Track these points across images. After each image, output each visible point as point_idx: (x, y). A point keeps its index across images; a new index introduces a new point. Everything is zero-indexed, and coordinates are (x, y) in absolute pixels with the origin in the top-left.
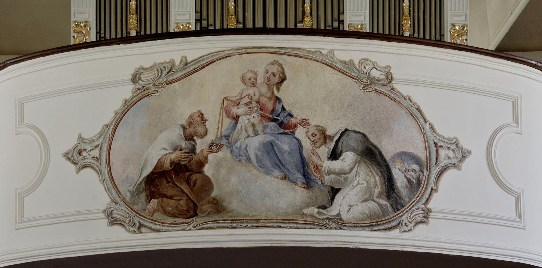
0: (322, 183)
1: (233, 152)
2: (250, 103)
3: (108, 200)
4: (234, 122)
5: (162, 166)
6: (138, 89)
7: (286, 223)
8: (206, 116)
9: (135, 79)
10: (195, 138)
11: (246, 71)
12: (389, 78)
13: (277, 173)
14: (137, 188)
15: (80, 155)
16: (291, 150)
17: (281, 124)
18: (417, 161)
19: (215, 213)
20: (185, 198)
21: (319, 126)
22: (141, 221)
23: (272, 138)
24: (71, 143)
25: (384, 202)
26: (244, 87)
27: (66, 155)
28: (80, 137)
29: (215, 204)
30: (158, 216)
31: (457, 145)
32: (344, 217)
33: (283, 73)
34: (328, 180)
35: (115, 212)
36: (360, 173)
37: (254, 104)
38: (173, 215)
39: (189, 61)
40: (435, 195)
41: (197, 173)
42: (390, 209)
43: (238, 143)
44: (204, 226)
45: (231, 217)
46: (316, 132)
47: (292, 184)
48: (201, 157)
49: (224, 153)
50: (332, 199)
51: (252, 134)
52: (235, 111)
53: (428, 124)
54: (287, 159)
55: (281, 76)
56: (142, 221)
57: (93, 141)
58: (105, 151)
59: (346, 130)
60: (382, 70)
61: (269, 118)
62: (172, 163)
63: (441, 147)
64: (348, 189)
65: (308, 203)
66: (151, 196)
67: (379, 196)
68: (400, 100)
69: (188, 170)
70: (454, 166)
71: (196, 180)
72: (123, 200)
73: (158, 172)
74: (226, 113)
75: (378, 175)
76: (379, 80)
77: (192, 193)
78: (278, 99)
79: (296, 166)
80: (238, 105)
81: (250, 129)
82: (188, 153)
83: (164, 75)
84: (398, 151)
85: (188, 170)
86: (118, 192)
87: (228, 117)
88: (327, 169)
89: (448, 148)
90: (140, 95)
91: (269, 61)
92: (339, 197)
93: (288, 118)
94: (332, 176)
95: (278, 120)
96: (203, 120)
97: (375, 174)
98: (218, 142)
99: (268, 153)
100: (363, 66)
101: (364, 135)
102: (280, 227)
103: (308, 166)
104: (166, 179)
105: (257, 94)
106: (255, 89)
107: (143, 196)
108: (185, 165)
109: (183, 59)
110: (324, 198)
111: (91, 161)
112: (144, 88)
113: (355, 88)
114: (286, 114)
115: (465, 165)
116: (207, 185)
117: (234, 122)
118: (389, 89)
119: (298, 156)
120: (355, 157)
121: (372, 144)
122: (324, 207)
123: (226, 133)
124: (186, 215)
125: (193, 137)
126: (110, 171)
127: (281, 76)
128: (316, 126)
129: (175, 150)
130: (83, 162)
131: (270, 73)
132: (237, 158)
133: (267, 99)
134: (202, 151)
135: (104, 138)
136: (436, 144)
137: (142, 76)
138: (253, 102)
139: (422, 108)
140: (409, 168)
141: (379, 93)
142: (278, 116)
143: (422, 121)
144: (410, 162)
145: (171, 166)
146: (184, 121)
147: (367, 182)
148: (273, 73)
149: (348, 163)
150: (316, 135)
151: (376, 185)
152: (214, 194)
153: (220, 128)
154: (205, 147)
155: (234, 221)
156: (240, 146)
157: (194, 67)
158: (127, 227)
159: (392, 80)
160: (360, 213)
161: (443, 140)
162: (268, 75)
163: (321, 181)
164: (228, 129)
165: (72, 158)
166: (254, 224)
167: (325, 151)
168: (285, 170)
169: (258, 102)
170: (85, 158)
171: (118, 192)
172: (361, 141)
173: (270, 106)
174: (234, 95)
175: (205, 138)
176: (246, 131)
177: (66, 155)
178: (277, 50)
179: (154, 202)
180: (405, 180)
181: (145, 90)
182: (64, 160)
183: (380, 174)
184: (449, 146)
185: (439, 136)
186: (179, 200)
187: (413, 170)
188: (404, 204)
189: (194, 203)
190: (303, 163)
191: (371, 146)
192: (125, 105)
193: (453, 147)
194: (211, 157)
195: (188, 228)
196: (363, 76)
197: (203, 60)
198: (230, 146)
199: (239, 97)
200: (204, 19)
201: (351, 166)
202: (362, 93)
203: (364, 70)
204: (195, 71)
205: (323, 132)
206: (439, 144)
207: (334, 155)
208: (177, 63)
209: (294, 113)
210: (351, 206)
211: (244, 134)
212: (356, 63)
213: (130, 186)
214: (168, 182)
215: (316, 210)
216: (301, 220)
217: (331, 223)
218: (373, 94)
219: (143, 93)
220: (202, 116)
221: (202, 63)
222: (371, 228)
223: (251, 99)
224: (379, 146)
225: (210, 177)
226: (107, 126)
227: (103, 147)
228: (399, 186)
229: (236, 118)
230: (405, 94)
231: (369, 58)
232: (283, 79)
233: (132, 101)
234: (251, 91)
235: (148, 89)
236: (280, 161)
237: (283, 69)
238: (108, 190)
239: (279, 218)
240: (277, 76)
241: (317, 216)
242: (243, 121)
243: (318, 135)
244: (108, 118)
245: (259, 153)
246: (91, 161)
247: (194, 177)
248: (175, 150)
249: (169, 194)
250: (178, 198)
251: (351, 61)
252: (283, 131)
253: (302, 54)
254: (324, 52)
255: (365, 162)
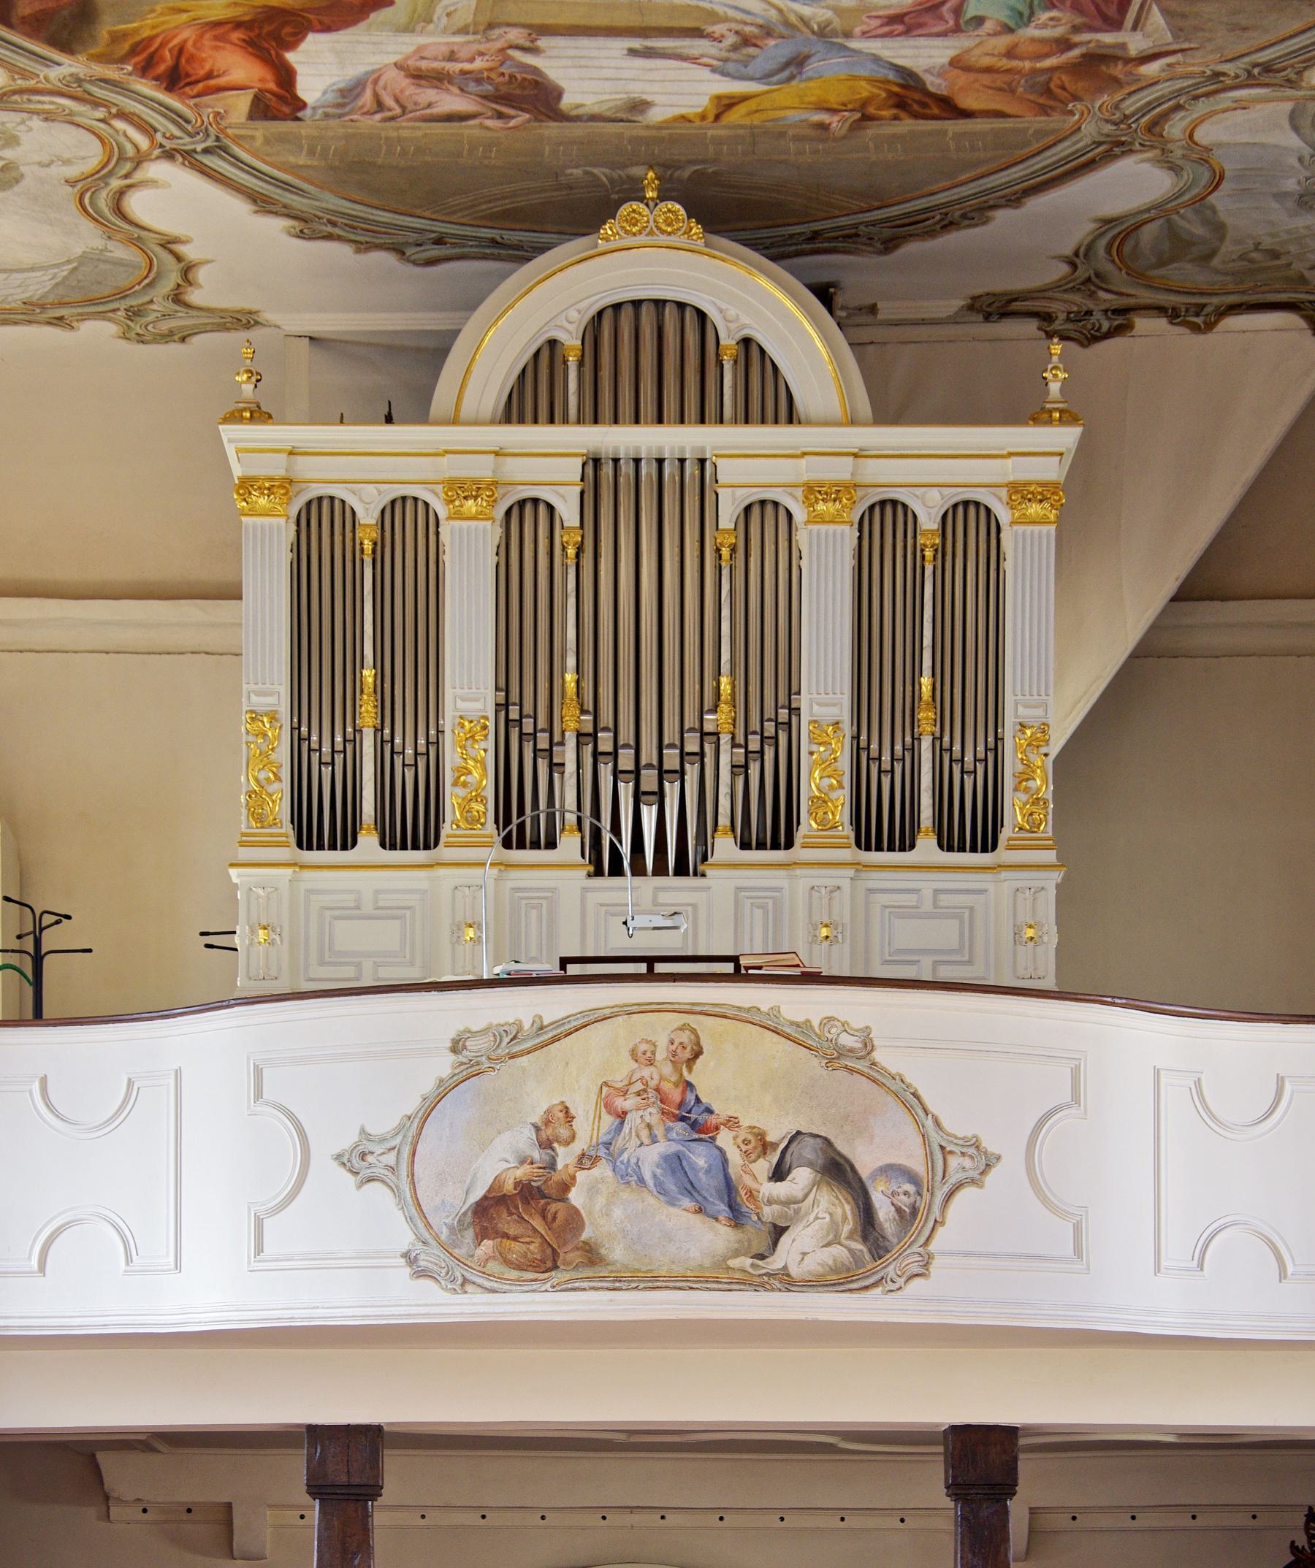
0: (759, 1219)
1: (617, 1170)
2: (645, 1091)
3: (410, 1237)
4: (618, 1121)
5: (501, 1187)
6: (462, 1064)
7: (700, 1282)
8: (572, 1111)
9: (457, 1047)
10: (555, 1145)
11: (638, 1040)
12: (868, 1046)
13: (687, 1203)
14: (459, 1221)
15: (363, 1160)
16: (710, 1166)
17: (694, 1126)
18: (913, 1178)
19: (587, 1266)
20: (538, 1240)
21: (754, 1127)
22: (465, 1273)
23: (680, 1147)
24: (347, 1140)
25: (858, 1246)
26: (636, 1065)
27: (338, 1157)
28: (363, 1131)
29: (587, 1251)
30: (494, 1267)
31: (977, 1147)
32: (795, 1271)
33: (698, 1044)
34: (769, 1212)
35: (422, 1257)
36: (819, 1202)
37: (651, 1093)
38: (519, 1268)
39: (545, 1023)
40: (940, 1231)
41: (559, 1200)
42: (867, 1257)
43: (625, 1155)
44: (569, 1286)
45: (612, 1271)
46: (750, 1137)
47: (711, 1220)
48: (565, 1177)
49: (602, 1171)
50: (775, 1243)
51: (646, 1141)
52: (620, 1103)
53: (930, 1116)
54: (702, 1179)
55: (695, 1048)
56: (468, 1275)
57: (383, 1140)
58: (406, 1156)
59: (799, 1133)
60: (856, 1033)
61: (674, 1115)
62: (517, 1183)
63: (951, 1152)
64: (800, 1227)
65: (737, 1250)
66: (482, 1235)
67: (849, 1237)
68: (885, 1081)
69: (544, 1197)
70: (973, 1182)
71: (556, 1213)
72: (436, 1237)
73: (494, 1197)
74: (606, 1106)
75: (848, 1203)
76: (851, 1050)
77: (549, 1232)
78: (689, 1085)
79: (718, 1191)
80: (625, 1093)
81: (644, 1134)
82: (544, 1168)
83: (504, 1043)
84: (880, 1164)
85: (544, 1197)
86: (428, 1225)
87: (609, 1113)
88: (767, 1195)
89: (963, 1154)
90: (465, 1073)
91: (676, 1025)
92: (785, 1240)
93: (705, 1116)
94: (776, 1207)
95: (689, 1118)
96: (569, 1117)
97: (843, 1201)
98: (592, 1153)
99: (673, 1172)
100: (826, 1029)
101: (827, 1140)
102: (691, 1288)
103: (737, 1192)
104: (508, 1209)
105: (656, 1077)
106: (652, 1068)
107: (470, 1234)
108: (538, 1188)
109: (537, 1019)
110: (760, 1244)
111: (382, 1171)
112: (472, 1063)
113: (814, 1065)
114: (702, 1108)
115: (990, 1179)
116: (575, 1221)
117: (618, 1121)
118: (868, 1064)
119: (721, 1176)
120: (812, 1176)
121: (839, 1154)
122: (762, 1257)
123: (605, 1139)
124: (539, 1267)
125: (551, 1143)
126: (415, 1190)
127: (695, 1048)
128: (750, 1127)
129: (522, 1162)
130: (368, 1172)
131: (676, 1044)
132: (622, 1177)
133: (671, 1086)
134: (566, 1166)
135: (404, 1136)
136: (942, 1148)
137: (468, 1043)
138: (649, 1090)
139: (921, 1092)
140: (899, 1190)
141: (851, 1071)
142: (689, 1112)
143: (920, 1112)
144: (900, 1180)
145: (515, 1189)
146: (537, 1118)
147: (831, 1214)
148: (681, 1043)
149: (801, 1186)
150: (750, 1142)
151: (845, 1218)
152: (585, 1236)
153: (595, 1132)
154: (572, 1160)
155: (617, 1279)
156: (629, 1160)
157: (555, 1033)
158: (443, 1282)
159: (872, 1050)
160: (819, 1264)
161: (955, 1141)
162: (674, 1047)
163: (758, 1214)
164: (609, 1133)
165: (348, 1164)
166: (650, 1284)
167: (764, 1166)
168: (700, 1198)
169: (657, 1090)
170: (370, 1166)
171: (428, 1225)
172: (821, 1149)
173: (676, 1095)
174: (619, 1078)
175: (572, 1145)
176: (638, 1136)
177: (338, 1157)
178: (688, 1007)
179: (488, 1244)
180: (893, 1209)
181: (473, 1066)
182: (335, 1164)
183: (850, 1199)
184: (964, 1150)
185: (949, 1135)
186: (528, 1243)
187: (906, 1193)
188: (889, 1248)
189: (553, 1249)
190: (729, 1189)
191: (838, 1158)
192: (439, 1086)
193: (972, 1151)
194: (581, 1176)
195: (543, 1289)
196: (826, 1045)
197: (569, 1022)
198: (613, 1159)
199: (626, 1082)
200: (515, 704)
201: (806, 1191)
202: (824, 1072)
203: (828, 1035)
204: (556, 1039)
205: (761, 1136)
206: (948, 1149)
207: (779, 1174)
208: (527, 1025)
209: (714, 1107)
210: (804, 1254)
211: (635, 1141)
212: (816, 1024)
213: (447, 1216)
214: (511, 1214)
215: (749, 1261)
216: (724, 1276)
217: (772, 1281)
218: (842, 1074)
219: (470, 1070)
220: (566, 1110)
221: (567, 1027)
222: (836, 1288)
223: (647, 1085)
224: (850, 1156)
225: (579, 1207)
226: (409, 1118)
227: (402, 1150)
228: (882, 1220)
229: (622, 1116)
230: (893, 1071)
231: (836, 1016)
232: (697, 1053)
233: (451, 1081)
234: (646, 1072)
235: (478, 1063)
236: (692, 1184)
237: (697, 1037)
238: (410, 1220)
239: (689, 1273)
240: (689, 1048)
241: (751, 1270)
242: (633, 1120)
243: (753, 1141)
244: (412, 1104)
245: (659, 1171)
246: (382, 1171)
247: (553, 1207)
248: (522, 1162)
249: (512, 1232)
250: (528, 1240)
251: (808, 1021)
252: (696, 1136)
253: (729, 1013)
254: (764, 1008)
255: (829, 1184)
